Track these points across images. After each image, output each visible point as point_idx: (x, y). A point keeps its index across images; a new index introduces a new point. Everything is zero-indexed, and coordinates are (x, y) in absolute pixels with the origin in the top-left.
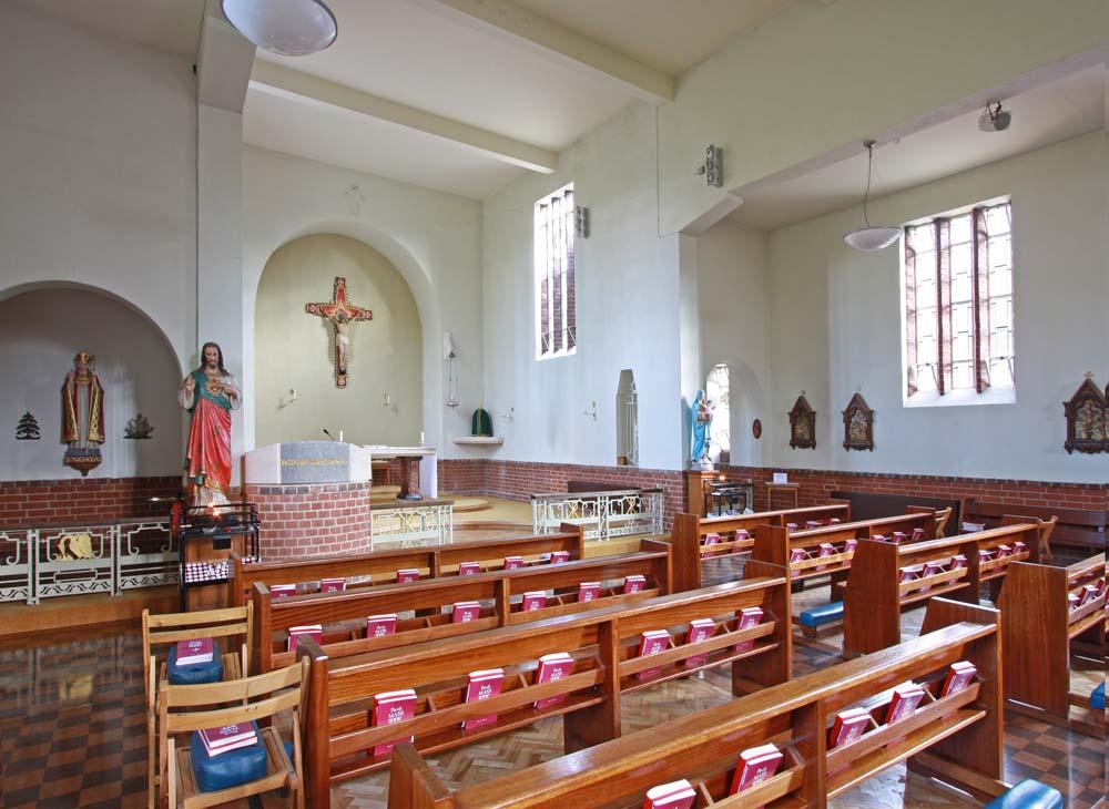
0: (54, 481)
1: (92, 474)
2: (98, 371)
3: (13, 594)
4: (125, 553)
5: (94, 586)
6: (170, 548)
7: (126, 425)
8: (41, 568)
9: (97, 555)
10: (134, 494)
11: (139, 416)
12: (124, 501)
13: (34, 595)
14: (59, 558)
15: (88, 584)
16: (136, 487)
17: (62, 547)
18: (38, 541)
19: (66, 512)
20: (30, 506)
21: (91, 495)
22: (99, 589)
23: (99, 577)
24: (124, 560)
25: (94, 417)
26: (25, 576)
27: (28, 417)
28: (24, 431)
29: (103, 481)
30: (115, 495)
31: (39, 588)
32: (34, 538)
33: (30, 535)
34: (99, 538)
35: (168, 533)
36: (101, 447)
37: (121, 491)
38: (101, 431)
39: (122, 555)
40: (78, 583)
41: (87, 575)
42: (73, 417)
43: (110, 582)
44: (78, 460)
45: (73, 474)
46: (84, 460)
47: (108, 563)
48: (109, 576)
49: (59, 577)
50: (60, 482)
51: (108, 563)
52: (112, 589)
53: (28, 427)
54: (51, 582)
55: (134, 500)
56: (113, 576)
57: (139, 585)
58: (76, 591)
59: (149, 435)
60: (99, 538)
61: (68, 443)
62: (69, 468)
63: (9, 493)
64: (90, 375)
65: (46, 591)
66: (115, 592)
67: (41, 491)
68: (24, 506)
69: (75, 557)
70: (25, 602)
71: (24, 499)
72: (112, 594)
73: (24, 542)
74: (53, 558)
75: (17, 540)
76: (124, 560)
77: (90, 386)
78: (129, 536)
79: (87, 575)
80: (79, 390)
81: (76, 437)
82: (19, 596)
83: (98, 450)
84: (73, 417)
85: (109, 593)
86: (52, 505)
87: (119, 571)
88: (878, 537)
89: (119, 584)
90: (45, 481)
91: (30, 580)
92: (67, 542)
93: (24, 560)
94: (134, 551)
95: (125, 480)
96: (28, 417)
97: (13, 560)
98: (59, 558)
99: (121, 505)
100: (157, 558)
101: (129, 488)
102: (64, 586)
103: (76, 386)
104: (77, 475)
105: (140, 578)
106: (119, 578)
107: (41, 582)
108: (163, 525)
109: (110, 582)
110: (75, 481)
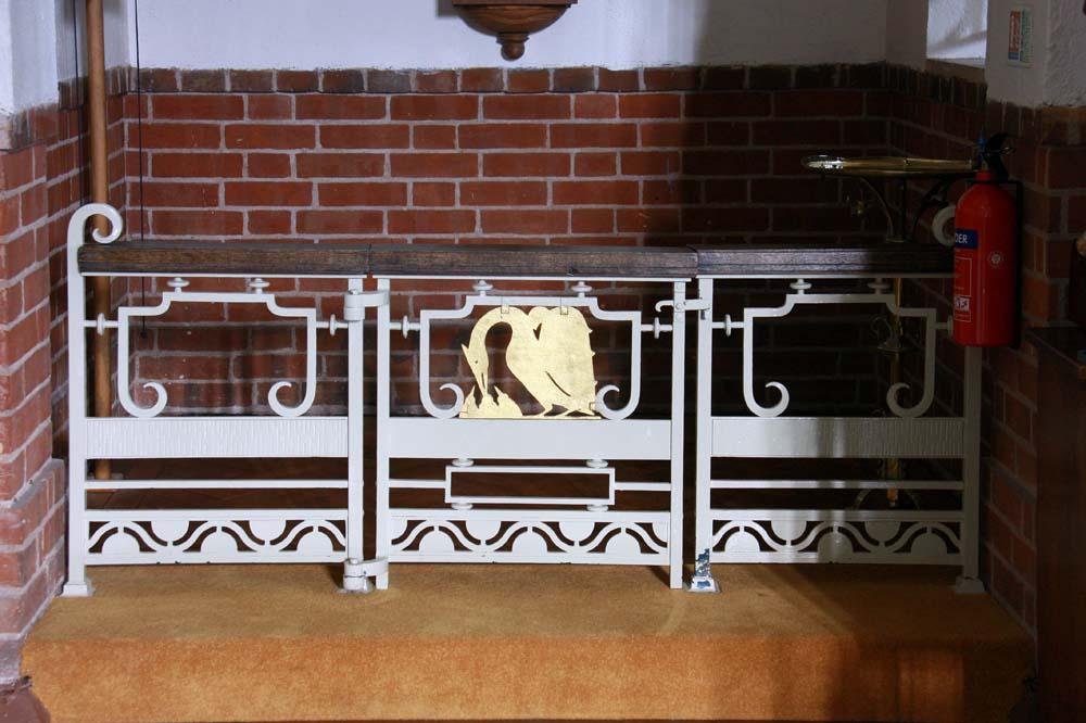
0: (404, 75)
1: (545, 51)
3: (292, 536)
4: (728, 403)
5: (600, 537)
9: (616, 401)
10: (691, 135)
13: (369, 552)
14: (464, 404)
15: (576, 524)
16: (694, 108)
17: (476, 354)
18: (385, 326)
19: (445, 193)
20: (329, 166)
21: (533, 136)
22: (624, 552)
23: (625, 502)
24: (724, 437)
26: (338, 467)
29: (575, 79)
30: (624, 136)
31: (391, 521)
32: (371, 313)
33: (357, 303)
34: (626, 327)
37: (639, 122)
39: (717, 410)
41: (579, 485)
43: (668, 524)
47: (658, 440)
48: (661, 502)
49: (464, 484)
50: (427, 79)
51: (658, 440)
52: (672, 558)
54: (434, 500)
55: (691, 163)
56: (677, 501)
57: (786, 555)
58: (529, 550)
60: (626, 327)
63: (254, 114)
65: (413, 536)
66: (688, 576)
67: (360, 110)
68: (308, 166)
70: (336, 572)
71: (302, 137)
72: (676, 580)
73: (334, 325)
74: (445, 399)
75: (634, 317)
76: (724, 437)
78: (747, 326)
79: (579, 485)
82: (315, 549)
86: (402, 165)
87: (705, 484)
88: (962, 303)
89: (705, 539)
90: (373, 73)
91: (354, 484)
92: (500, 337)
93: (333, 399)
94: (767, 398)
95: (658, 77)
98: (464, 404)
101: (666, 109)
102: (485, 524)
104: (481, 51)
105: (787, 522)
106: (705, 514)
107: (399, 499)
109: (668, 524)
110: (478, 78)
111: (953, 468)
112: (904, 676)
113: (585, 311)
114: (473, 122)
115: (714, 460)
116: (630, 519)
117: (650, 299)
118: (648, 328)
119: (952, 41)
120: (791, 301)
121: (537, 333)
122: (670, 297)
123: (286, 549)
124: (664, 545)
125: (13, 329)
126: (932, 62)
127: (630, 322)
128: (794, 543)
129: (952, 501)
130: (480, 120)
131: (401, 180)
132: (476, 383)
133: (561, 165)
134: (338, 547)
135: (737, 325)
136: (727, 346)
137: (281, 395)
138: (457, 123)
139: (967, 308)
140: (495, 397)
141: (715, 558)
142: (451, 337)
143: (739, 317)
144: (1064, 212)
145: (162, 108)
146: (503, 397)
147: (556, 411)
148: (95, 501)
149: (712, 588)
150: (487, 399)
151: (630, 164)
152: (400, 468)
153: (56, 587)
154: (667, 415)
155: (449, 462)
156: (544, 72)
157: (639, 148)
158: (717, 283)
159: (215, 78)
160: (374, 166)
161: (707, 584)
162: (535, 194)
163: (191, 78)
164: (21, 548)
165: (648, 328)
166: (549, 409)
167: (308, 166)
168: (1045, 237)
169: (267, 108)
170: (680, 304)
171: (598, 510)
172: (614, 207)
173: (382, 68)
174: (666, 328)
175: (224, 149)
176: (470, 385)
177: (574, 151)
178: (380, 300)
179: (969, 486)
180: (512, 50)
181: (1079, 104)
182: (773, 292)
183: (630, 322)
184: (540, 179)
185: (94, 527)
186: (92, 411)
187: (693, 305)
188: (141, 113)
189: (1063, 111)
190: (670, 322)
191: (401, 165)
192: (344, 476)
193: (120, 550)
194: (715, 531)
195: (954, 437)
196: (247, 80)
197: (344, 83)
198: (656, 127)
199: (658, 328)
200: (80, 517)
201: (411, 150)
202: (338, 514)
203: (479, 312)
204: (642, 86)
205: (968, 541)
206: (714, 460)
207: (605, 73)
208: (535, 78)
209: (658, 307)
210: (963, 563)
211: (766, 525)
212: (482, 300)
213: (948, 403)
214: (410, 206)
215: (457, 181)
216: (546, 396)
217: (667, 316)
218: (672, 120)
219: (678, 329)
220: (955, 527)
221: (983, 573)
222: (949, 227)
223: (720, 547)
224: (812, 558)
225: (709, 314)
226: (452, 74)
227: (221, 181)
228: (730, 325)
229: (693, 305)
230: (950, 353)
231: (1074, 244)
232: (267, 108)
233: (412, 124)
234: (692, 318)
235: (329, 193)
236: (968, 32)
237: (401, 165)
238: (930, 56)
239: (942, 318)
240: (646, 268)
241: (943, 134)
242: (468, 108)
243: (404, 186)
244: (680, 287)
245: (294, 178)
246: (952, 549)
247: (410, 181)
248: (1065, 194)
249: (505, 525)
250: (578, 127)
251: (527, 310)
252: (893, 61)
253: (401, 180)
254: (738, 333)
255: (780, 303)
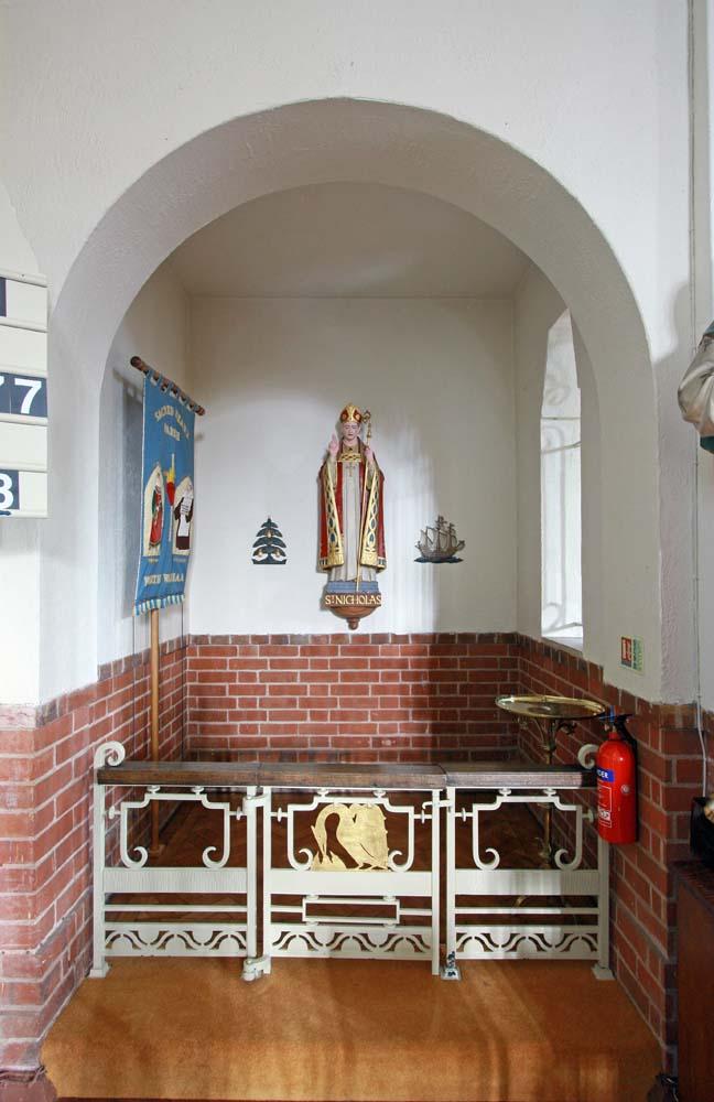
0: (306, 637)
1: (367, 626)
2: (376, 446)
3: (217, 939)
4: (464, 862)
6: (577, 861)
7: (419, 537)
8: (277, 881)
9: (400, 861)
11: (441, 521)
12: (416, 676)
16: (434, 651)
17: (319, 832)
18: (268, 815)
20: (273, 678)
21: (362, 664)
23: (405, 921)
24: (466, 882)
25: (369, 522)
26: (240, 899)
27: (269, 525)
28: (264, 550)
30: (403, 664)
31: (272, 931)
35: (572, 814)
36: (379, 577)
37: (410, 658)
38: (380, 549)
39: (458, 866)
40: (356, 931)
42: (336, 521)
44: (343, 601)
45: (335, 625)
46: (351, 601)
47: (423, 884)
48: (427, 921)
49: (314, 910)
50: (316, 638)
51: (423, 884)
53: (269, 544)
54: (295, 919)
57: (499, 954)
59: (457, 555)
61: (329, 569)
62: (329, 614)
64: (362, 448)
65: (285, 940)
66: (443, 963)
68: (264, 677)
69: (350, 863)
71: (261, 664)
74: (302, 859)
75: (410, 810)
76: (466, 882)
77: (362, 466)
78: (475, 815)
80: (345, 472)
81: (340, 558)
82: (230, 949)
83: (375, 584)
84: (336, 521)
85: (428, 964)
89: (453, 945)
90: (293, 636)
92: (333, 821)
93: (238, 860)
94: (487, 859)
95: (417, 637)
96: (269, 525)
97: (216, 857)
99: (410, 684)
100: (541, 883)
103: (340, 466)
104: (339, 626)
105: (500, 933)
106: (453, 929)
107: (277, 918)
108: (559, 793)
110: (338, 638)
111: (591, 901)
112: (582, 1073)
113: (382, 806)
114: (336, 657)
115: (457, 897)
116: (411, 931)
117: (419, 799)
118: (418, 817)
119: (553, 628)
120: (500, 800)
121: (354, 819)
122: (430, 799)
123: (219, 932)
124: (428, 947)
125: (39, 839)
126: (544, 639)
127: (407, 814)
128: (503, 946)
129: (593, 920)
130: (339, 657)
131: (304, 684)
132: (319, 849)
133: (375, 677)
134: (242, 947)
135: (469, 815)
136: (463, 827)
137: (210, 854)
138: (329, 658)
139: (608, 819)
140: (330, 857)
141: (458, 956)
142: (305, 821)
143: (469, 810)
144: (674, 768)
145: (205, 652)
146: (335, 857)
147: (366, 866)
148: (110, 917)
149: (456, 977)
150: (326, 858)
151: (406, 677)
152: (278, 899)
153: (84, 974)
154: (429, 869)
155: (305, 896)
156: (367, 635)
157: (410, 669)
158: (458, 792)
159: (224, 639)
160: (292, 677)
161: (454, 973)
162: (364, 690)
163: (215, 639)
164: (41, 980)
165: (418, 817)
166: (361, 865)
167: (264, 677)
168: (662, 784)
169: (247, 652)
170: (436, 803)
171: (390, 925)
172: (399, 696)
173: (296, 633)
174: (428, 817)
175: (228, 670)
176: (315, 849)
177: (380, 671)
178: (265, 802)
179: (602, 910)
180: (353, 625)
181: (680, 704)
182: (490, 795)
183: (407, 814)
184: (365, 683)
185: (108, 933)
186: (108, 863)
187: (444, 804)
188: (194, 654)
189: (672, 707)
190: (431, 813)
191: (305, 677)
192: (595, 905)
193: (123, 949)
194: (458, 939)
195: (594, 882)
196: (238, 639)
197: (280, 639)
198: (418, 660)
199: (424, 817)
200: (100, 926)
201: (309, 670)
202: (241, 927)
203: (321, 806)
204: (410, 641)
205: (603, 944)
206: (457, 897)
207: (394, 636)
208: (363, 638)
209: (424, 807)
210: (599, 958)
211: (487, 936)
212: (323, 799)
213: (590, 862)
214: (308, 696)
215: (329, 684)
216: (359, 858)
217: (429, 810)
218: (423, 657)
219: (435, 817)
220: (595, 936)
221: (612, 964)
222: (589, 757)
223: (461, 949)
224: (513, 956)
225: (453, 809)
226: (327, 636)
227: (227, 684)
228: (465, 815)
229: (444, 804)
230: (590, 843)
231: (703, 815)
232: (247, 652)
233: (309, 658)
234: (443, 811)
235: (274, 690)
236: (559, 625)
237: (305, 677)
238: (544, 635)
239: (585, 811)
240: (417, 779)
241: (552, 674)
242: (333, 651)
243: (306, 687)
244: (436, 793)
245: (258, 683)
246: (593, 949)
247: (308, 684)
248: (674, 759)
249: (337, 935)
250: (382, 660)
251: (348, 805)
252: (521, 633)
253: (304, 684)
254: (470, 819)
255: (492, 801)
